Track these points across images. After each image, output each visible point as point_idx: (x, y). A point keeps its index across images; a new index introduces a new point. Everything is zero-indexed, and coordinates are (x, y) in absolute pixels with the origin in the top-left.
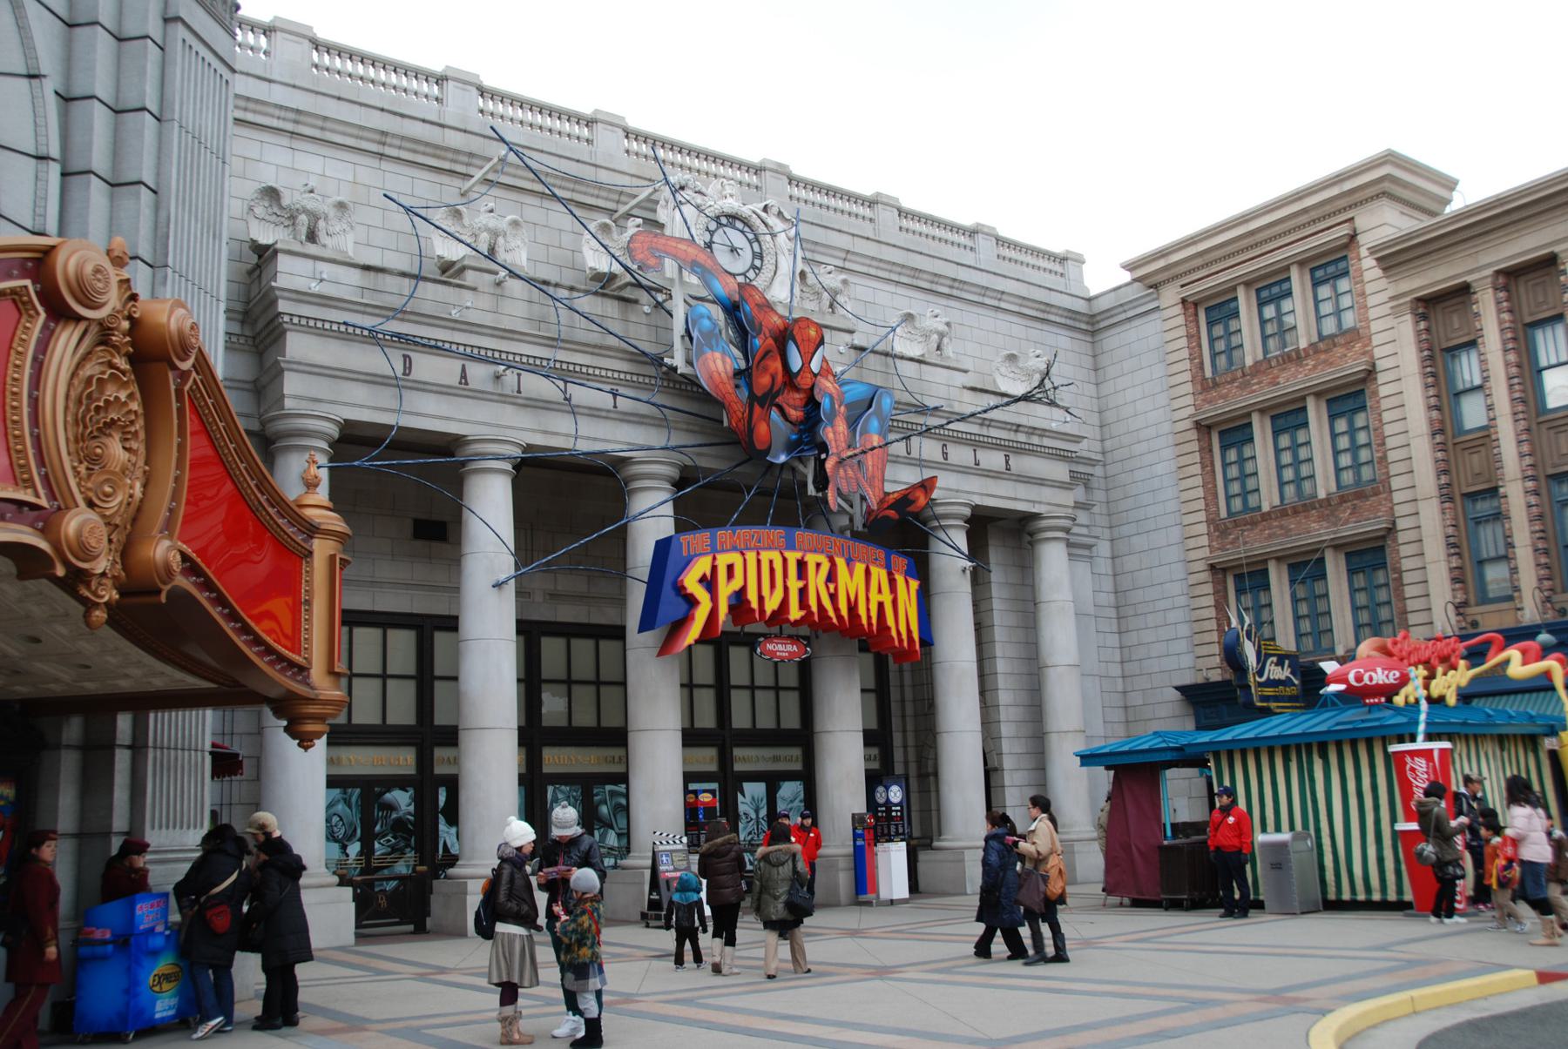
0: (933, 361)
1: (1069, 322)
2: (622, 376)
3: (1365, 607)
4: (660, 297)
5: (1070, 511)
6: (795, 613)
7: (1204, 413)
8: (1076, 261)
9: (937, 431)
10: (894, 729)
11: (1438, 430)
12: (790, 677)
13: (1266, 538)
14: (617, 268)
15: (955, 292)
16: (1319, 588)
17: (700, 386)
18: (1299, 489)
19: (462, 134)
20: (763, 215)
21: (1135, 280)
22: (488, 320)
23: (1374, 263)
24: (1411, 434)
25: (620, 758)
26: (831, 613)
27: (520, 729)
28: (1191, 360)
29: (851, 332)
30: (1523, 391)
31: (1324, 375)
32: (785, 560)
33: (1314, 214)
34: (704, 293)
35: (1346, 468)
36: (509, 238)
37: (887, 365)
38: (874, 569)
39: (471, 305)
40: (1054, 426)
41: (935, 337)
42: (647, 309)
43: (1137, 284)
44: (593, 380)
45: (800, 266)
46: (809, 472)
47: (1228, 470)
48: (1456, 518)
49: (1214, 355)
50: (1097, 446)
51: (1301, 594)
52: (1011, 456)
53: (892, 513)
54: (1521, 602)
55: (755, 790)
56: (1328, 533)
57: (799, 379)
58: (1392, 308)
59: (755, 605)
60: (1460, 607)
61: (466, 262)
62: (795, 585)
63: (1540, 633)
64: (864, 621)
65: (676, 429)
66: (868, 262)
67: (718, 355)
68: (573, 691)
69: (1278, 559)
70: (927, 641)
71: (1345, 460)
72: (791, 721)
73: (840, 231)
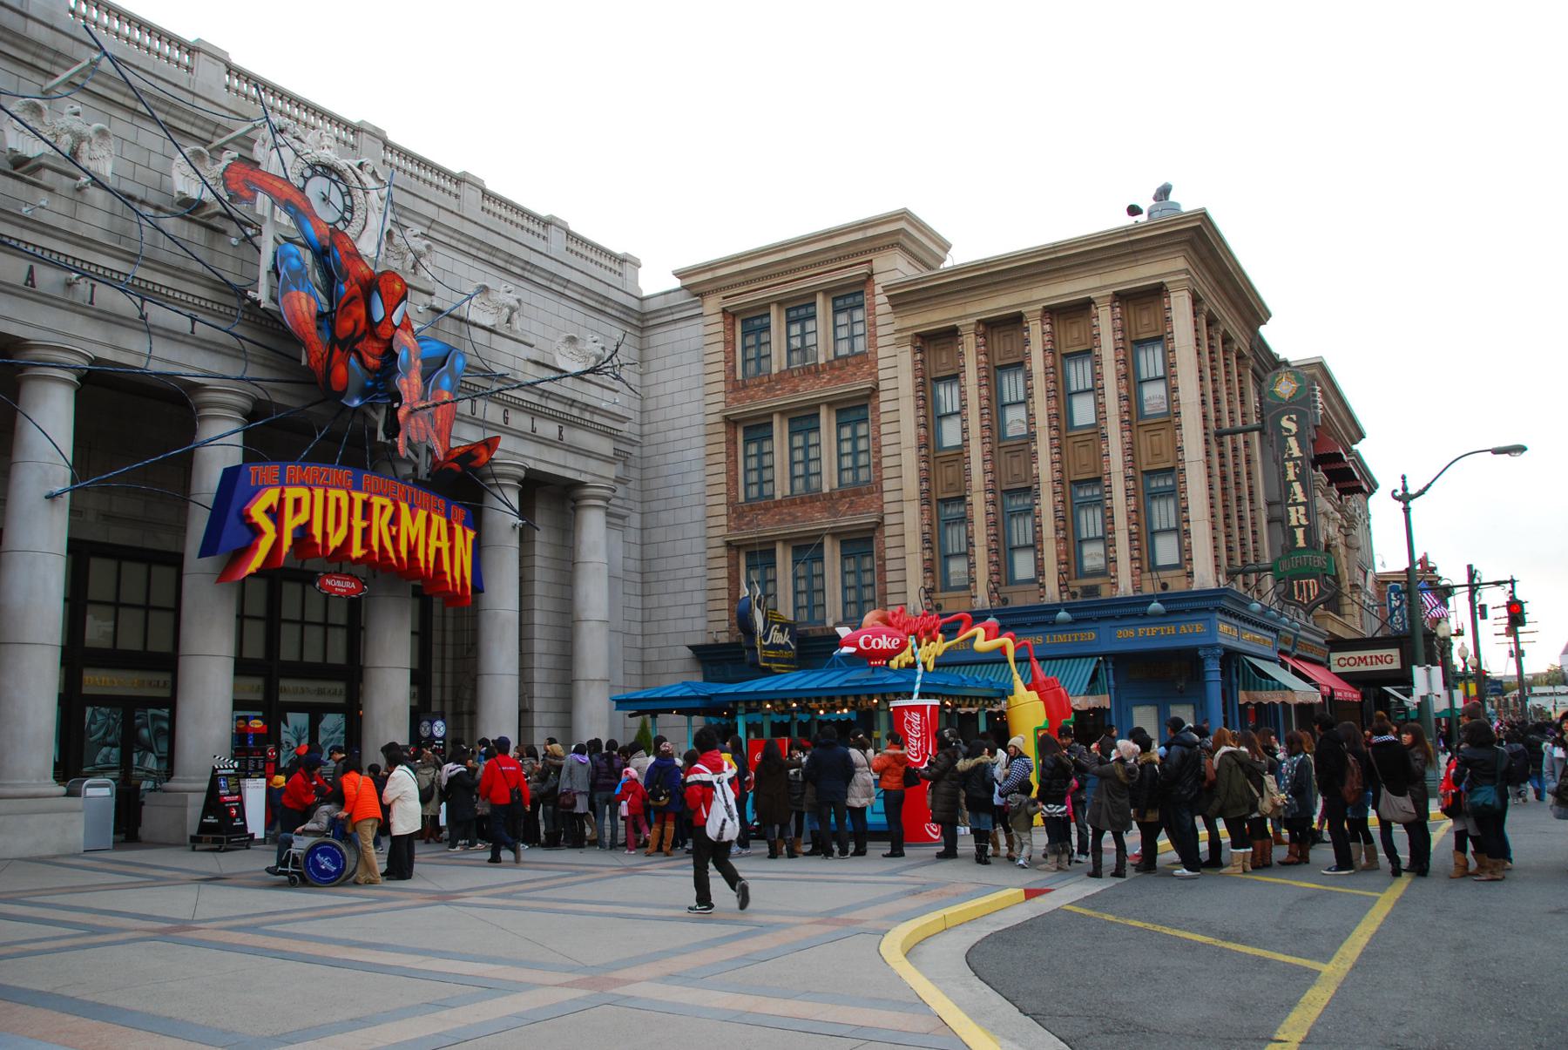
0: (503, 332)
1: (622, 316)
2: (203, 303)
3: (853, 587)
4: (250, 232)
5: (612, 483)
6: (357, 551)
7: (733, 410)
8: (634, 264)
9: (497, 395)
10: (433, 670)
11: (923, 444)
12: (339, 615)
13: (776, 523)
14: (207, 196)
15: (526, 274)
16: (816, 568)
17: (284, 326)
18: (807, 483)
19: (49, 30)
20: (358, 171)
21: (684, 287)
22: (64, 224)
23: (886, 300)
24: (903, 446)
25: (165, 682)
26: (392, 554)
27: (62, 647)
28: (726, 363)
29: (431, 294)
30: (990, 420)
31: (837, 389)
32: (351, 500)
33: (841, 253)
34: (294, 235)
35: (847, 469)
36: (95, 147)
37: (460, 330)
38: (435, 517)
39: (47, 206)
40: (604, 405)
41: (507, 310)
42: (234, 241)
43: (684, 291)
44: (171, 303)
45: (388, 226)
46: (380, 419)
47: (749, 461)
48: (931, 519)
49: (745, 361)
50: (637, 429)
51: (801, 573)
52: (564, 427)
53: (456, 466)
54: (976, 591)
55: (298, 720)
56: (828, 523)
57: (379, 329)
58: (896, 339)
59: (319, 539)
60: (929, 592)
61: (43, 161)
62: (358, 525)
63: (1060, 611)
64: (422, 564)
65: (253, 362)
66: (451, 233)
67: (303, 295)
68: (120, 615)
69: (785, 542)
70: (478, 587)
71: (847, 462)
72: (338, 655)
73: (427, 201)
